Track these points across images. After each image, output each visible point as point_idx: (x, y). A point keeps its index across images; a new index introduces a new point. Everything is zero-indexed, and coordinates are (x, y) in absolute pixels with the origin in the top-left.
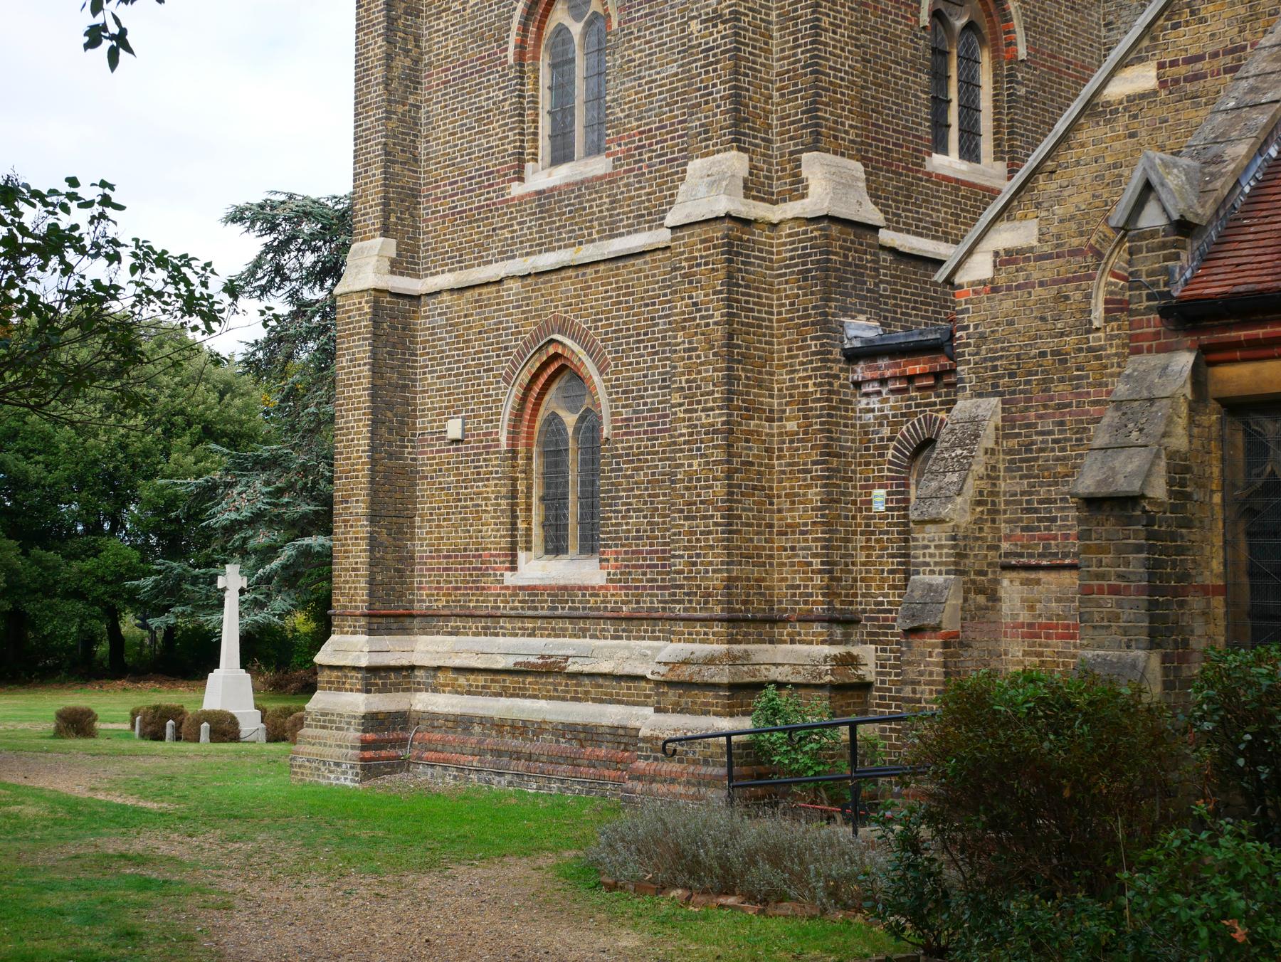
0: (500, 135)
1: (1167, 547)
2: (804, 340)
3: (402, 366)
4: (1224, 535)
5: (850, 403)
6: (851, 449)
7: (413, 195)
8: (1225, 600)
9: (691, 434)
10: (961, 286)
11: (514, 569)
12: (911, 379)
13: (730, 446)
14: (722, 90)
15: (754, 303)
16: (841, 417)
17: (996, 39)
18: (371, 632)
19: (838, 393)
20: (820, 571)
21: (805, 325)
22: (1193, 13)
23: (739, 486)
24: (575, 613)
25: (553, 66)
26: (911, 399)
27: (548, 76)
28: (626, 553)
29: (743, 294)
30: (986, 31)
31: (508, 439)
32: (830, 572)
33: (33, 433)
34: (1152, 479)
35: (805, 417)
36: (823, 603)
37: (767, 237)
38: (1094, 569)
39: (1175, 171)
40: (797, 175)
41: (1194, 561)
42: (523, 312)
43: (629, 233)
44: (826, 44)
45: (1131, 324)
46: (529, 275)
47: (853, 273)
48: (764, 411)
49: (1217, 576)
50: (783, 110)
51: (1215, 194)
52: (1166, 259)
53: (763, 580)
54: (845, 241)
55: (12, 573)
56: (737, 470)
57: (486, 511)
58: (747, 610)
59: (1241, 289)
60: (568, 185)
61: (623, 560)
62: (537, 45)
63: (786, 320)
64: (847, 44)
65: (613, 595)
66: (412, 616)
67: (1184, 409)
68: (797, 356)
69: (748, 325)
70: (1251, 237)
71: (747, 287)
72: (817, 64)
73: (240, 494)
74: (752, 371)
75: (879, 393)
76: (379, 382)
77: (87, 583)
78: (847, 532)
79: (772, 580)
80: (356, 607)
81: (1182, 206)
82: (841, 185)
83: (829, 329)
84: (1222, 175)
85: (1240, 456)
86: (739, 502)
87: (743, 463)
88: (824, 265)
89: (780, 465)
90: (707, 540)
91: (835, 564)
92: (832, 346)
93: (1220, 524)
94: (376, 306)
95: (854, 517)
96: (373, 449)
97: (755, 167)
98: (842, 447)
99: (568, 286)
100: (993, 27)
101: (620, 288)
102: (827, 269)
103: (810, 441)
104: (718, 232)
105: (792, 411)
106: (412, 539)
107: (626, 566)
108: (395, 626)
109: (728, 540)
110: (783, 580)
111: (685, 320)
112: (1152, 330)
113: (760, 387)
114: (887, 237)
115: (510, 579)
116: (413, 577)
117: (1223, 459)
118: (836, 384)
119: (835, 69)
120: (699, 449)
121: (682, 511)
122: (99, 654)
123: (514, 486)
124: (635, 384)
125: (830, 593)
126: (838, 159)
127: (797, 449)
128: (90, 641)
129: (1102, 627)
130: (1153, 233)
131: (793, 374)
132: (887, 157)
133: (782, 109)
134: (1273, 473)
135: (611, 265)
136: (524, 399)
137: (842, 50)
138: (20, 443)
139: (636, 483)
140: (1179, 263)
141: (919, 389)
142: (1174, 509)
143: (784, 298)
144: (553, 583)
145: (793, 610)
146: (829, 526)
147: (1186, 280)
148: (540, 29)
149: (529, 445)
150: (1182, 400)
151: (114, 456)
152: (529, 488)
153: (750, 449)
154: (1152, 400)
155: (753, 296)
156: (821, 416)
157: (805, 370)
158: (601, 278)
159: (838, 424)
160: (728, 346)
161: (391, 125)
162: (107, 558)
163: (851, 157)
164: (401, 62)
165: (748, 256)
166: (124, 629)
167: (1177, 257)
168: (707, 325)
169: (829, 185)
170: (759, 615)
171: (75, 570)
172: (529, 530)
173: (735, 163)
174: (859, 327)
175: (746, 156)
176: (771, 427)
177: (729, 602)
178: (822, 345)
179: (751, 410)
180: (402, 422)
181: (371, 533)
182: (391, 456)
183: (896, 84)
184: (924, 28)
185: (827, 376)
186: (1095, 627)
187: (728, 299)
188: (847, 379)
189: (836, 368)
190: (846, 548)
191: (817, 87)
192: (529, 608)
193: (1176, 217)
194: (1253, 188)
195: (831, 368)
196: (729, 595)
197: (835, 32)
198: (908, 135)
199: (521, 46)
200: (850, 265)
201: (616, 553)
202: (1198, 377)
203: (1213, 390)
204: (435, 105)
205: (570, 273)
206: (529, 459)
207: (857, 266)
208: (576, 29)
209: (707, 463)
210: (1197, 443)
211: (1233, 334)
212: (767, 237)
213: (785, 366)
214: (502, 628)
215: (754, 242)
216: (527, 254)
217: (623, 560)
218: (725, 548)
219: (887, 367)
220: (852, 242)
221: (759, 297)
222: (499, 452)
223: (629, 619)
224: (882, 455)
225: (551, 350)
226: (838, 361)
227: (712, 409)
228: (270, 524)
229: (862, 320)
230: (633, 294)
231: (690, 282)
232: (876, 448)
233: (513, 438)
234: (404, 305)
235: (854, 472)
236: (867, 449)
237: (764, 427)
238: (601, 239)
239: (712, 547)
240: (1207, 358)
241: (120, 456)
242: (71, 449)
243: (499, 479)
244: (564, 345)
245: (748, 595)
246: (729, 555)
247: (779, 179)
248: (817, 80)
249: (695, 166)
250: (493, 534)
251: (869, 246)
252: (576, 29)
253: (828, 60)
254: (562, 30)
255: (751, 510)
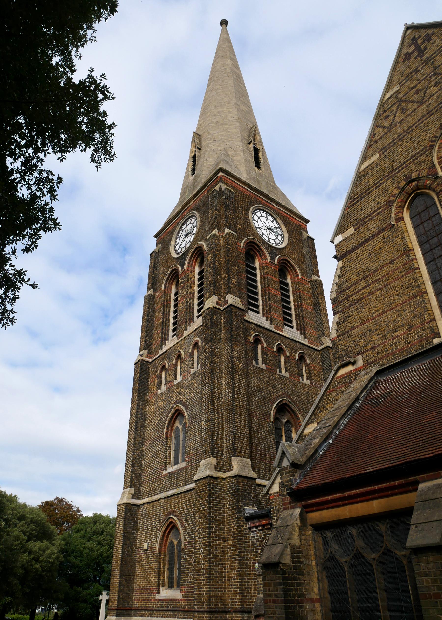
0: (161, 458)
1: (292, 583)
2: (233, 514)
3: (133, 527)
4: (318, 578)
5: (248, 534)
6: (248, 550)
7: (140, 476)
8: (321, 605)
9: (200, 546)
10: (271, 494)
11: (159, 593)
12: (264, 526)
13: (210, 550)
14: (209, 440)
15: (218, 503)
16: (244, 539)
17: (296, 425)
18: (117, 615)
19: (243, 531)
20: (239, 593)
21: (233, 509)
22: (324, 407)
23: (213, 563)
24: (173, 609)
25: (175, 438)
26: (264, 532)
27: (174, 441)
28: (187, 587)
29: (214, 500)
30: (293, 423)
31: (159, 549)
32: (242, 593)
34: (284, 556)
35: (234, 540)
36: (240, 605)
37: (222, 482)
38: (268, 592)
39: (294, 448)
40: (231, 464)
41: (306, 589)
42: (164, 509)
43: (190, 484)
44: (237, 426)
45: (282, 499)
46: (166, 497)
47: (247, 493)
48: (222, 538)
49: (316, 594)
50: (227, 445)
51: (307, 454)
52: (291, 476)
53: (222, 597)
54: (244, 483)
56: (212, 558)
57: (152, 573)
58: (216, 608)
59: (311, 485)
60: (176, 470)
61: (187, 590)
62: (171, 432)
63: (228, 508)
64: (244, 426)
65: (184, 602)
66: (132, 610)
67: (297, 529)
68: (231, 519)
69: (216, 510)
70: (319, 468)
71: (215, 498)
72: (235, 432)
74: (218, 525)
75: (256, 531)
76: (126, 532)
78: (248, 579)
79: (226, 597)
80: (114, 607)
81: (293, 458)
82: (243, 466)
83: (239, 510)
84: (310, 448)
85: (322, 547)
86: (213, 569)
87: (214, 555)
88: (238, 491)
89: (227, 556)
90: (203, 583)
91: (244, 590)
92: (241, 516)
93: (316, 573)
94: (126, 508)
95: (250, 574)
96: (122, 553)
97: (219, 462)
98: (245, 550)
99: (175, 500)
100: (295, 423)
101: (187, 500)
102: (238, 492)
103: (235, 547)
104: (206, 482)
105: (230, 537)
106: (133, 583)
107: (187, 592)
108: (126, 613)
109: (209, 582)
110: (229, 597)
111: (198, 509)
112: (288, 501)
113: (220, 530)
114: (258, 481)
115: (158, 597)
116: (133, 596)
117: (315, 548)
118: (242, 528)
119: (240, 433)
120: (202, 551)
121: (197, 572)
123: (160, 565)
124: (190, 530)
125: (242, 601)
126: (242, 459)
127: (232, 550)
129: (271, 617)
130: (286, 468)
131: (230, 526)
132: (262, 458)
133: (226, 445)
134: (331, 552)
135: (185, 494)
136: (163, 536)
137: (243, 427)
138: (74, 554)
139: (190, 563)
140: (294, 477)
141: (266, 529)
142: (295, 567)
143: (227, 502)
144: (168, 598)
145: (232, 608)
146: (241, 577)
147: (297, 483)
148: (172, 428)
149: (164, 551)
150: (296, 525)
152: (164, 565)
153: (217, 550)
154: (286, 526)
155: (218, 501)
156: (237, 539)
157: (233, 524)
158: (183, 498)
159: (244, 542)
160: (209, 517)
161: (134, 456)
163: (246, 458)
164: (139, 439)
165: (216, 488)
167: (294, 475)
168: (204, 510)
169: (239, 466)
170: (221, 610)
171: (85, 593)
172: (164, 580)
173: (212, 461)
174: (250, 510)
175: (215, 459)
176: (224, 543)
177: (210, 605)
178: (238, 516)
179: (218, 538)
180: (132, 544)
181: (120, 581)
182: (128, 555)
183: (264, 437)
184: (272, 422)
185: (239, 525)
186: (269, 617)
187: (209, 502)
188: (246, 526)
189: (242, 523)
190: (248, 585)
191: (235, 438)
192: (162, 607)
193: (291, 462)
194: (323, 453)
195: (240, 523)
196: (209, 602)
197: (240, 423)
198: (268, 452)
199: (167, 433)
200: (246, 490)
201: (185, 587)
202: (302, 516)
203: (309, 522)
204: (147, 451)
205: (175, 496)
206: (165, 556)
207: (248, 490)
208: (180, 427)
209: (204, 556)
210: (304, 542)
211: (311, 501)
212: (222, 482)
213: (228, 523)
214: (154, 614)
215: (218, 484)
216: (166, 491)
217: (187, 590)
218: (208, 585)
219: (257, 522)
220: (247, 483)
221: (220, 501)
222: (156, 554)
223: (187, 611)
224: (257, 552)
225: (170, 520)
226: (243, 521)
227: (205, 537)
229: (251, 507)
230: (190, 502)
231: (200, 497)
232: (256, 549)
233: (160, 549)
234: (135, 508)
235: (250, 558)
236: (253, 550)
237: (222, 543)
238: (183, 486)
239: (205, 585)
240: (306, 509)
243: (156, 562)
244: (173, 519)
245: (217, 602)
246: (209, 588)
247: (226, 465)
248: (235, 436)
249: (203, 462)
250: (154, 581)
251: (252, 484)
252: (180, 427)
253: (238, 430)
254: (177, 428)
255: (218, 572)
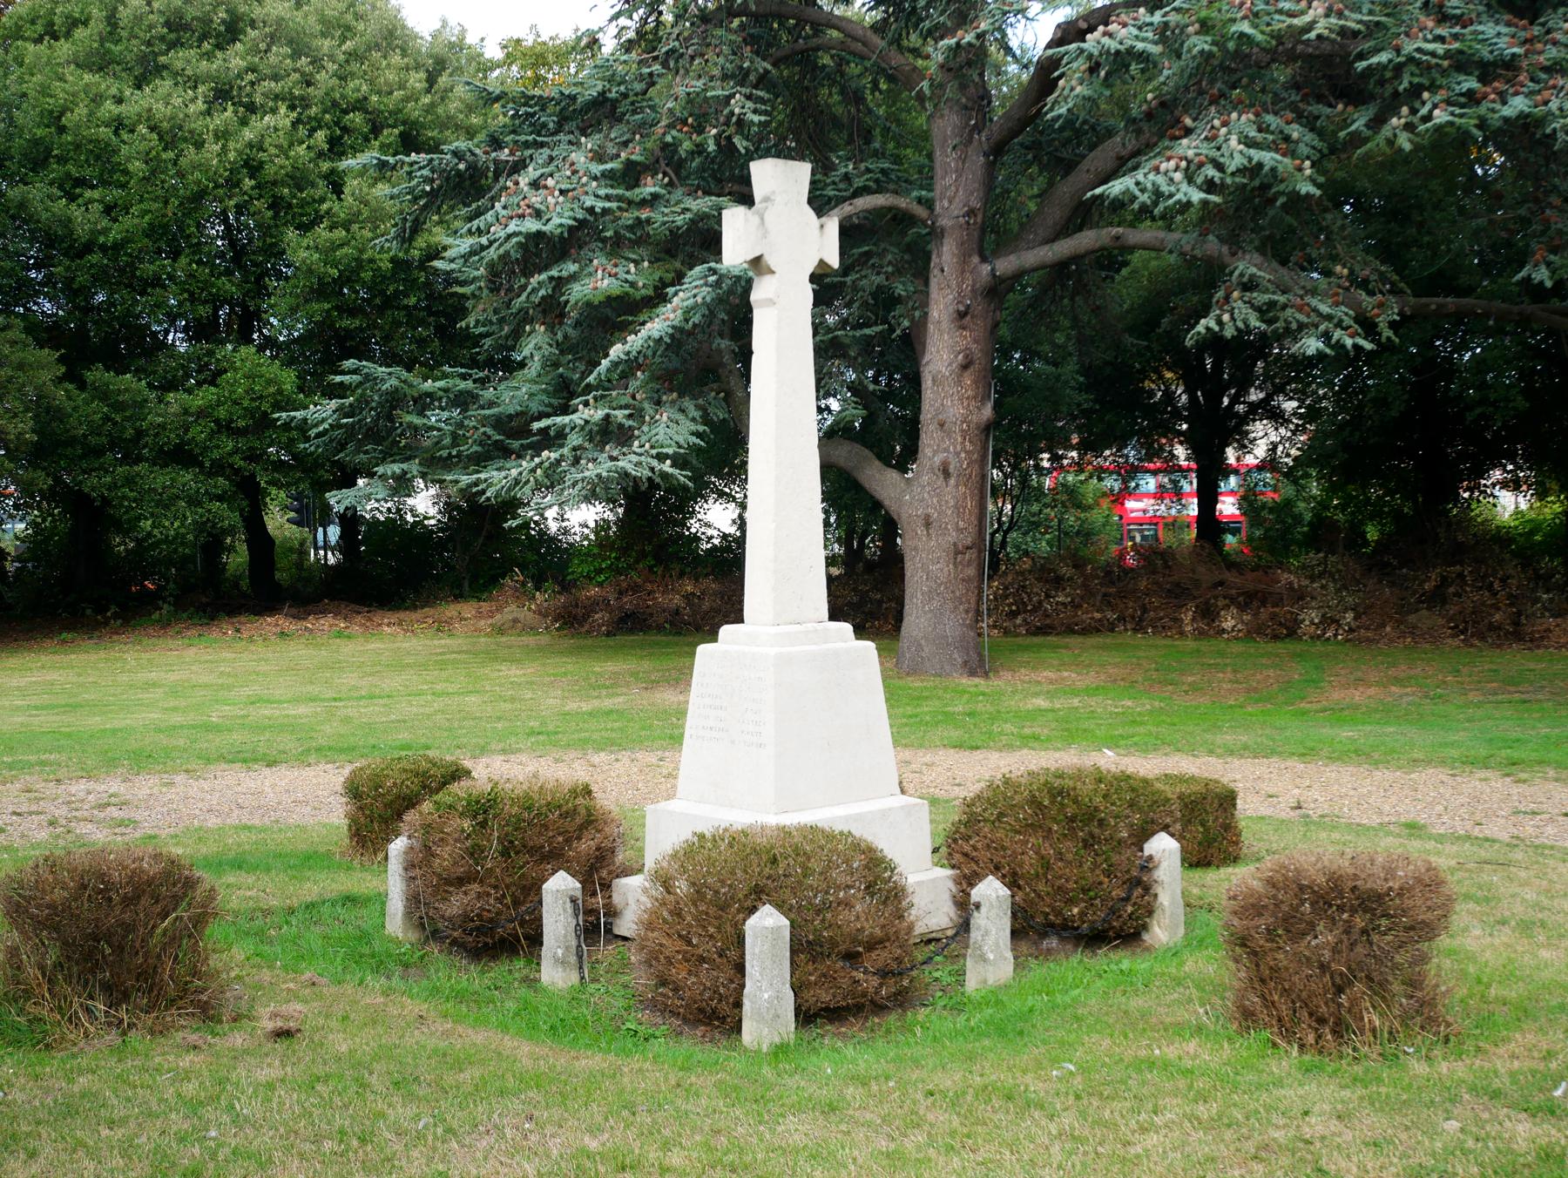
33: (78, 147)
55: (47, 414)
73: (535, 185)
77: (199, 433)
122: (231, 568)
128: (213, 545)
138: (55, 170)
151: (238, 184)
162: (236, 383)
166: (271, 526)
171: (174, 409)
228: (616, 247)
241: (248, 183)
242: (153, 172)
